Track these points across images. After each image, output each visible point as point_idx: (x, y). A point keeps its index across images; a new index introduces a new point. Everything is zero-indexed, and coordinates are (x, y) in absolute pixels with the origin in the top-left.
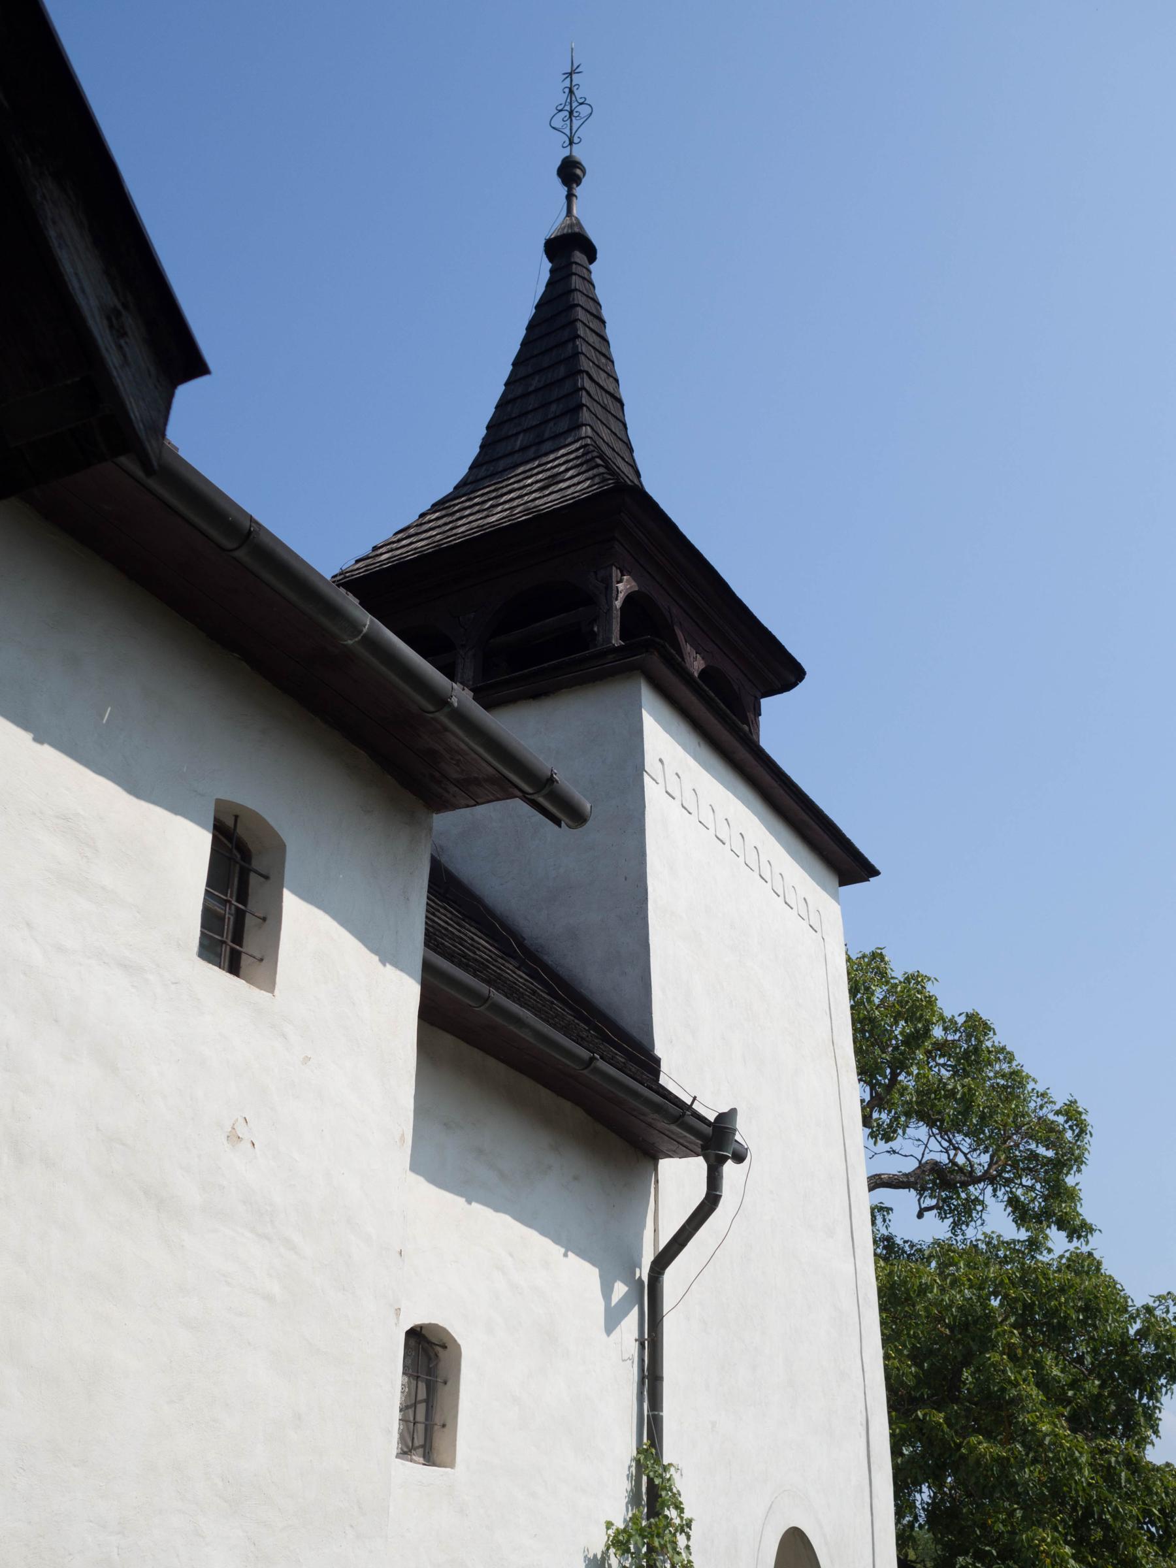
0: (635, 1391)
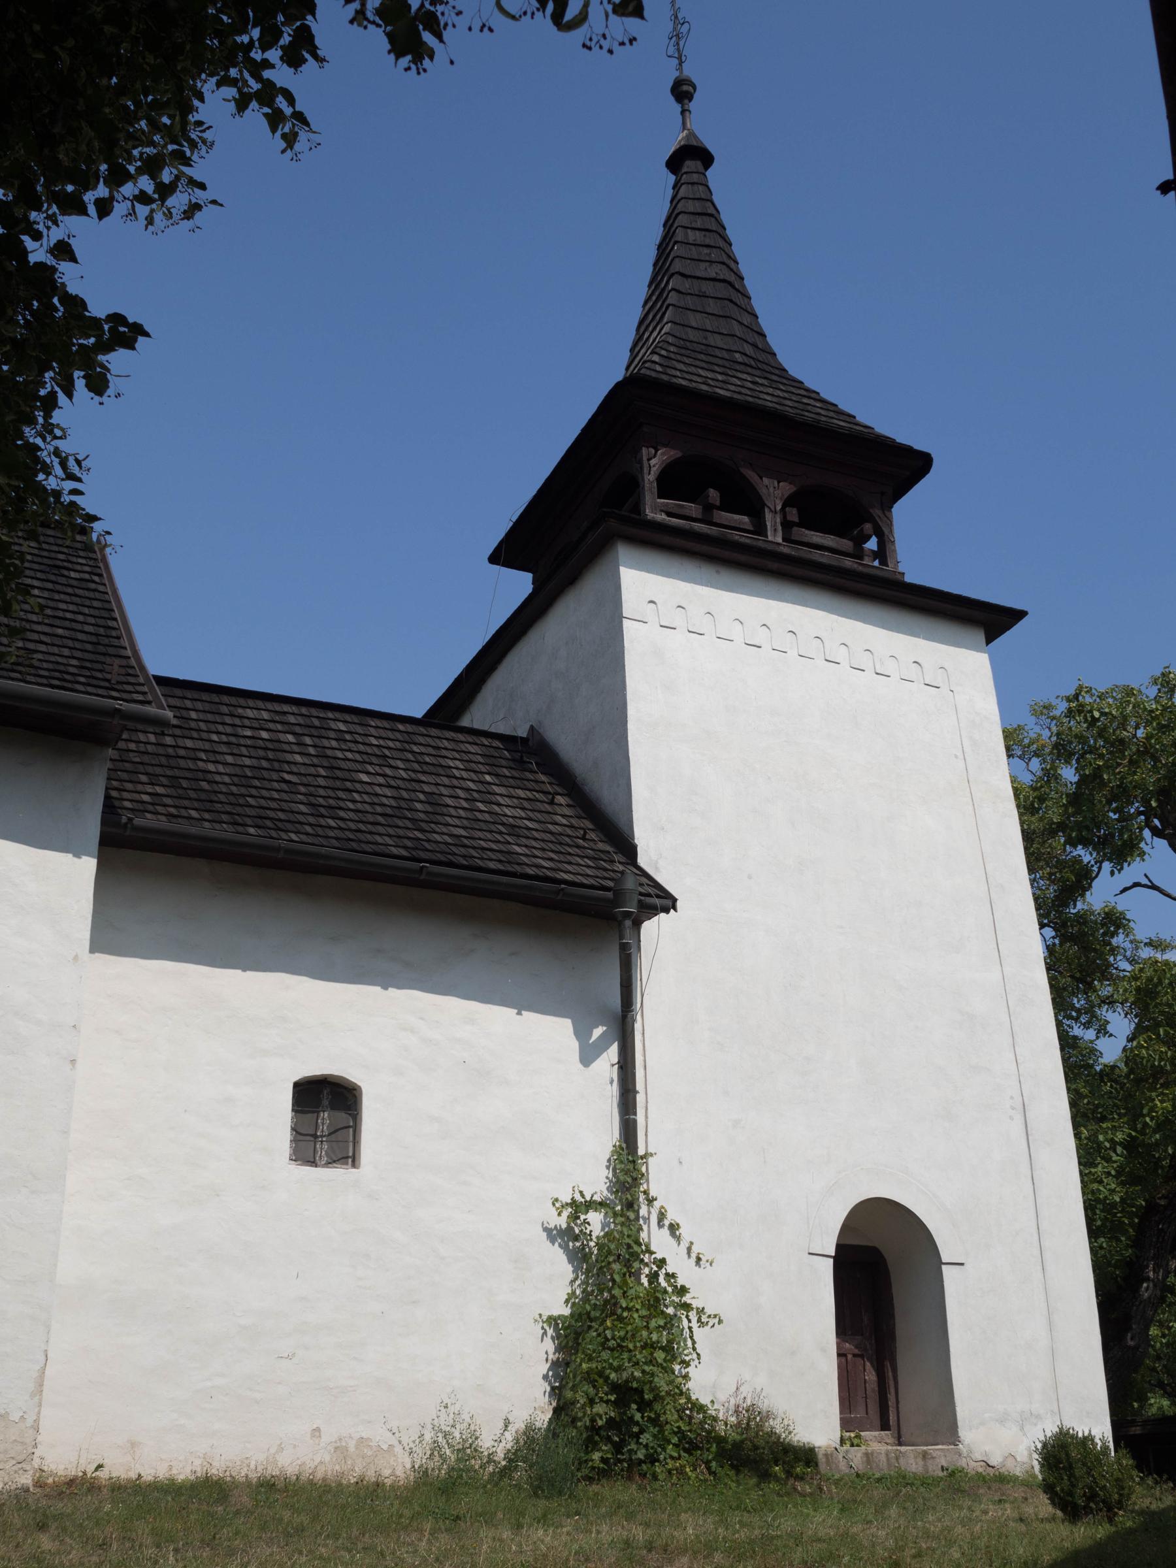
0: (616, 1101)
